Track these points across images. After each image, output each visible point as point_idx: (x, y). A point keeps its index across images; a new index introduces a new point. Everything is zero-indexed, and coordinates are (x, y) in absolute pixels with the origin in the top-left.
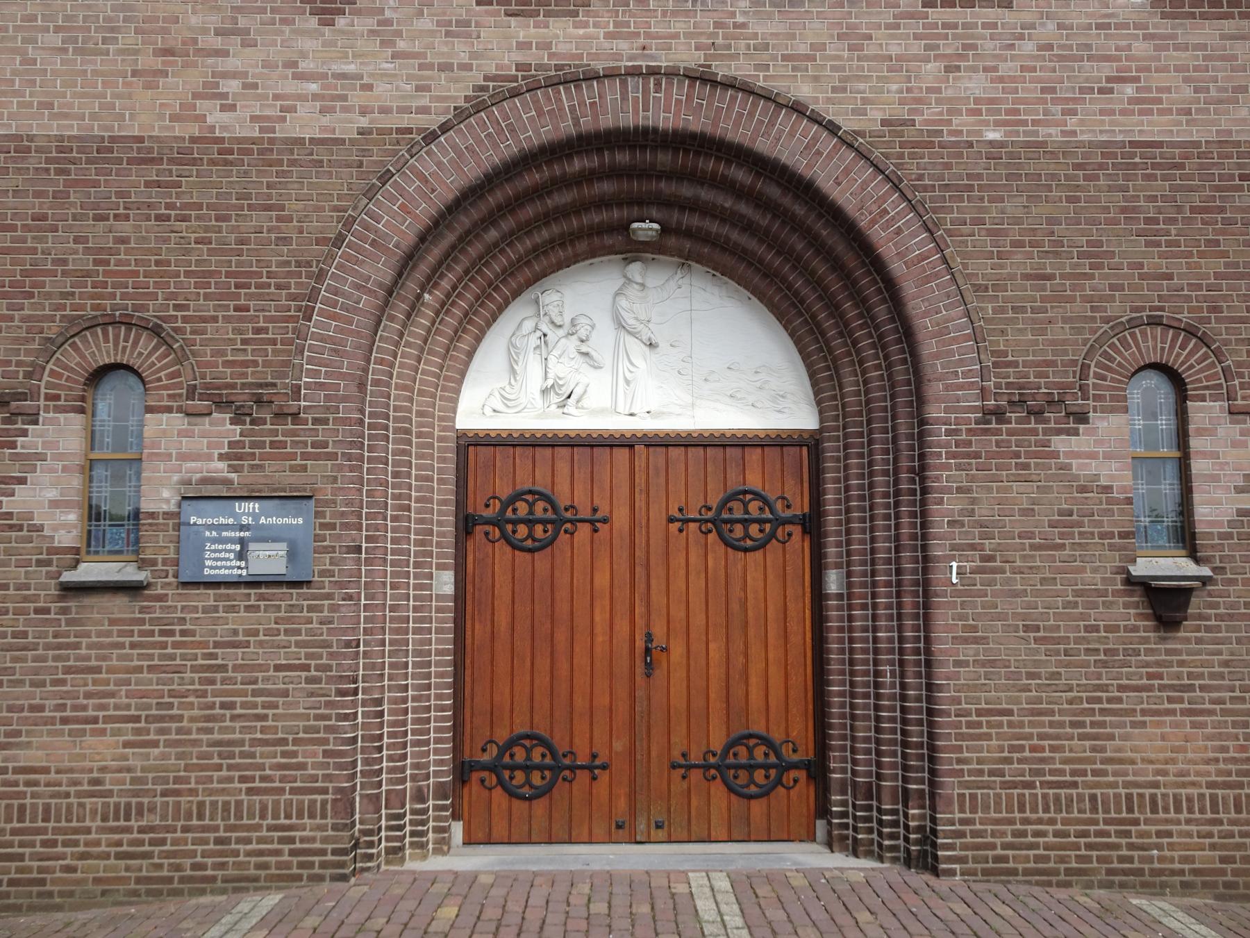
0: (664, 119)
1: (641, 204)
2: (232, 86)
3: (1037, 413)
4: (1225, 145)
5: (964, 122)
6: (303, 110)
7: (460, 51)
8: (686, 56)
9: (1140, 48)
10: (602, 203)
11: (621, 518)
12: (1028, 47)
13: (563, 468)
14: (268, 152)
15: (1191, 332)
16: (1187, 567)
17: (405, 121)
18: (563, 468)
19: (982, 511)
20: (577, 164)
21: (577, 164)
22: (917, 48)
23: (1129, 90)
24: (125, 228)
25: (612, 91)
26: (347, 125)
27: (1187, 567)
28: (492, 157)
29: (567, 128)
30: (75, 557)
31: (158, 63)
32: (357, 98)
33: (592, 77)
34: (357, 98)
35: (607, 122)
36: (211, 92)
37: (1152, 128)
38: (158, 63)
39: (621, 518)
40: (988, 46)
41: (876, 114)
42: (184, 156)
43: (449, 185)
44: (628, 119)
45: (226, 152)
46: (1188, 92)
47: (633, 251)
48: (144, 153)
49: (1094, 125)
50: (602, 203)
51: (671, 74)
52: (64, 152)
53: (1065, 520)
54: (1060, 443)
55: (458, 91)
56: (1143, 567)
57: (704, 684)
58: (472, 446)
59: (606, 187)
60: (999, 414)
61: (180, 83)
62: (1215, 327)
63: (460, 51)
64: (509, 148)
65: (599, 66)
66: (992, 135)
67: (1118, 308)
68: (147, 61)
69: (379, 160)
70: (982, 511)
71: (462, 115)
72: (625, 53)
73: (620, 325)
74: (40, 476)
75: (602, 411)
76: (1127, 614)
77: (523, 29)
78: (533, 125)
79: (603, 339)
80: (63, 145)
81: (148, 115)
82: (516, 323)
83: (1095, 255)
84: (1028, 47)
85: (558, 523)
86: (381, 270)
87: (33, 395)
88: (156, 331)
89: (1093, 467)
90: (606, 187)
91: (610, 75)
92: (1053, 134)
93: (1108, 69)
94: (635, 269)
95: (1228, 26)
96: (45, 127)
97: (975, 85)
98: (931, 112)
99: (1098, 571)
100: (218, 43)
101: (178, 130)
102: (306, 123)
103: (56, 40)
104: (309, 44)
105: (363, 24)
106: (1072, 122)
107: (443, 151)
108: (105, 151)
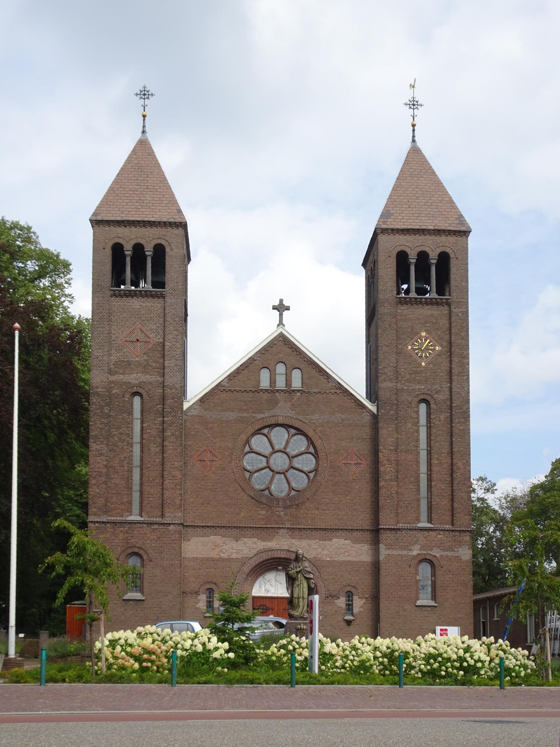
0: (283, 556)
1: (280, 565)
2: (224, 551)
3: (333, 597)
4: (360, 562)
5: (324, 558)
6: (234, 554)
7: (255, 546)
8: (286, 548)
9: (349, 547)
10: (274, 565)
11: (276, 609)
12: (334, 547)
13: (268, 602)
14: (229, 560)
15: (354, 587)
16: (352, 618)
17: (248, 556)
18: (268, 602)
19: (325, 610)
20: (271, 561)
21: (271, 561)
22: (318, 547)
23: (347, 553)
24: (210, 570)
25: (276, 553)
26: (240, 556)
27: (352, 618)
28: (259, 561)
29: (270, 557)
30: (205, 613)
31: (214, 547)
32: (241, 553)
33: (273, 550)
34: (241, 553)
35: (275, 556)
36: (221, 551)
37: (350, 559)
38: (214, 547)
39: (276, 609)
40: (328, 547)
41: (312, 556)
42: (218, 560)
43: (254, 564)
44: (278, 556)
45: (224, 560)
46: (355, 554)
47: (278, 570)
48: (213, 560)
49: (342, 558)
50: (274, 565)
51: (284, 550)
52: (202, 560)
53: (336, 612)
54: (336, 601)
55: (255, 552)
56: (346, 618)
57: (185, 252)
58: (254, 598)
59: (275, 563)
60: (328, 597)
61: (217, 550)
62: (357, 586)
63: (255, 546)
64: (262, 560)
65: (274, 549)
66: (328, 559)
67: (345, 583)
68: (213, 547)
69: (244, 561)
70: (325, 610)
71: (255, 555)
72: (278, 547)
73: (276, 580)
74: (201, 602)
75: (272, 593)
76: (344, 624)
77: (264, 543)
78: (265, 557)
79: (273, 582)
80: (202, 558)
81: (214, 554)
82: (260, 580)
83: (342, 576)
84: (334, 547)
85: (267, 609)
86: (244, 576)
87: (199, 592)
88: (215, 584)
89: (340, 605)
90: (275, 563)
91: (276, 550)
92: (336, 559)
93: (345, 550)
94: (278, 572)
95: (361, 545)
96: (199, 556)
97: (326, 552)
98: (319, 556)
99: (340, 618)
100: (222, 545)
101: (217, 557)
102: (234, 556)
103: (201, 544)
104: (235, 545)
105: (242, 542)
106: (339, 558)
107: (253, 560)
108: (207, 559)
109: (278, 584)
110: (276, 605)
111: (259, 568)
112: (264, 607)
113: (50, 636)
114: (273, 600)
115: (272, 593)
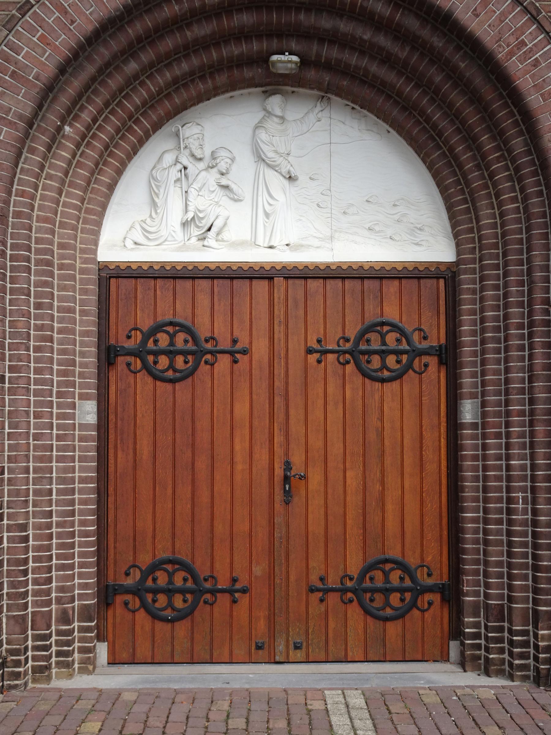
1: (281, 36)
11: (260, 349)
13: (203, 300)
18: (203, 300)
39: (260, 349)
58: (113, 276)
73: (260, 158)
75: (235, 245)
79: (243, 172)
82: (156, 158)
85: (198, 354)
86: (21, 103)
94: (275, 103)
109: (275, 180)
110: (262, 323)
111: (130, 52)
112: (395, 577)
113: (459, 664)
114: (241, 286)
115: (235, 245)
